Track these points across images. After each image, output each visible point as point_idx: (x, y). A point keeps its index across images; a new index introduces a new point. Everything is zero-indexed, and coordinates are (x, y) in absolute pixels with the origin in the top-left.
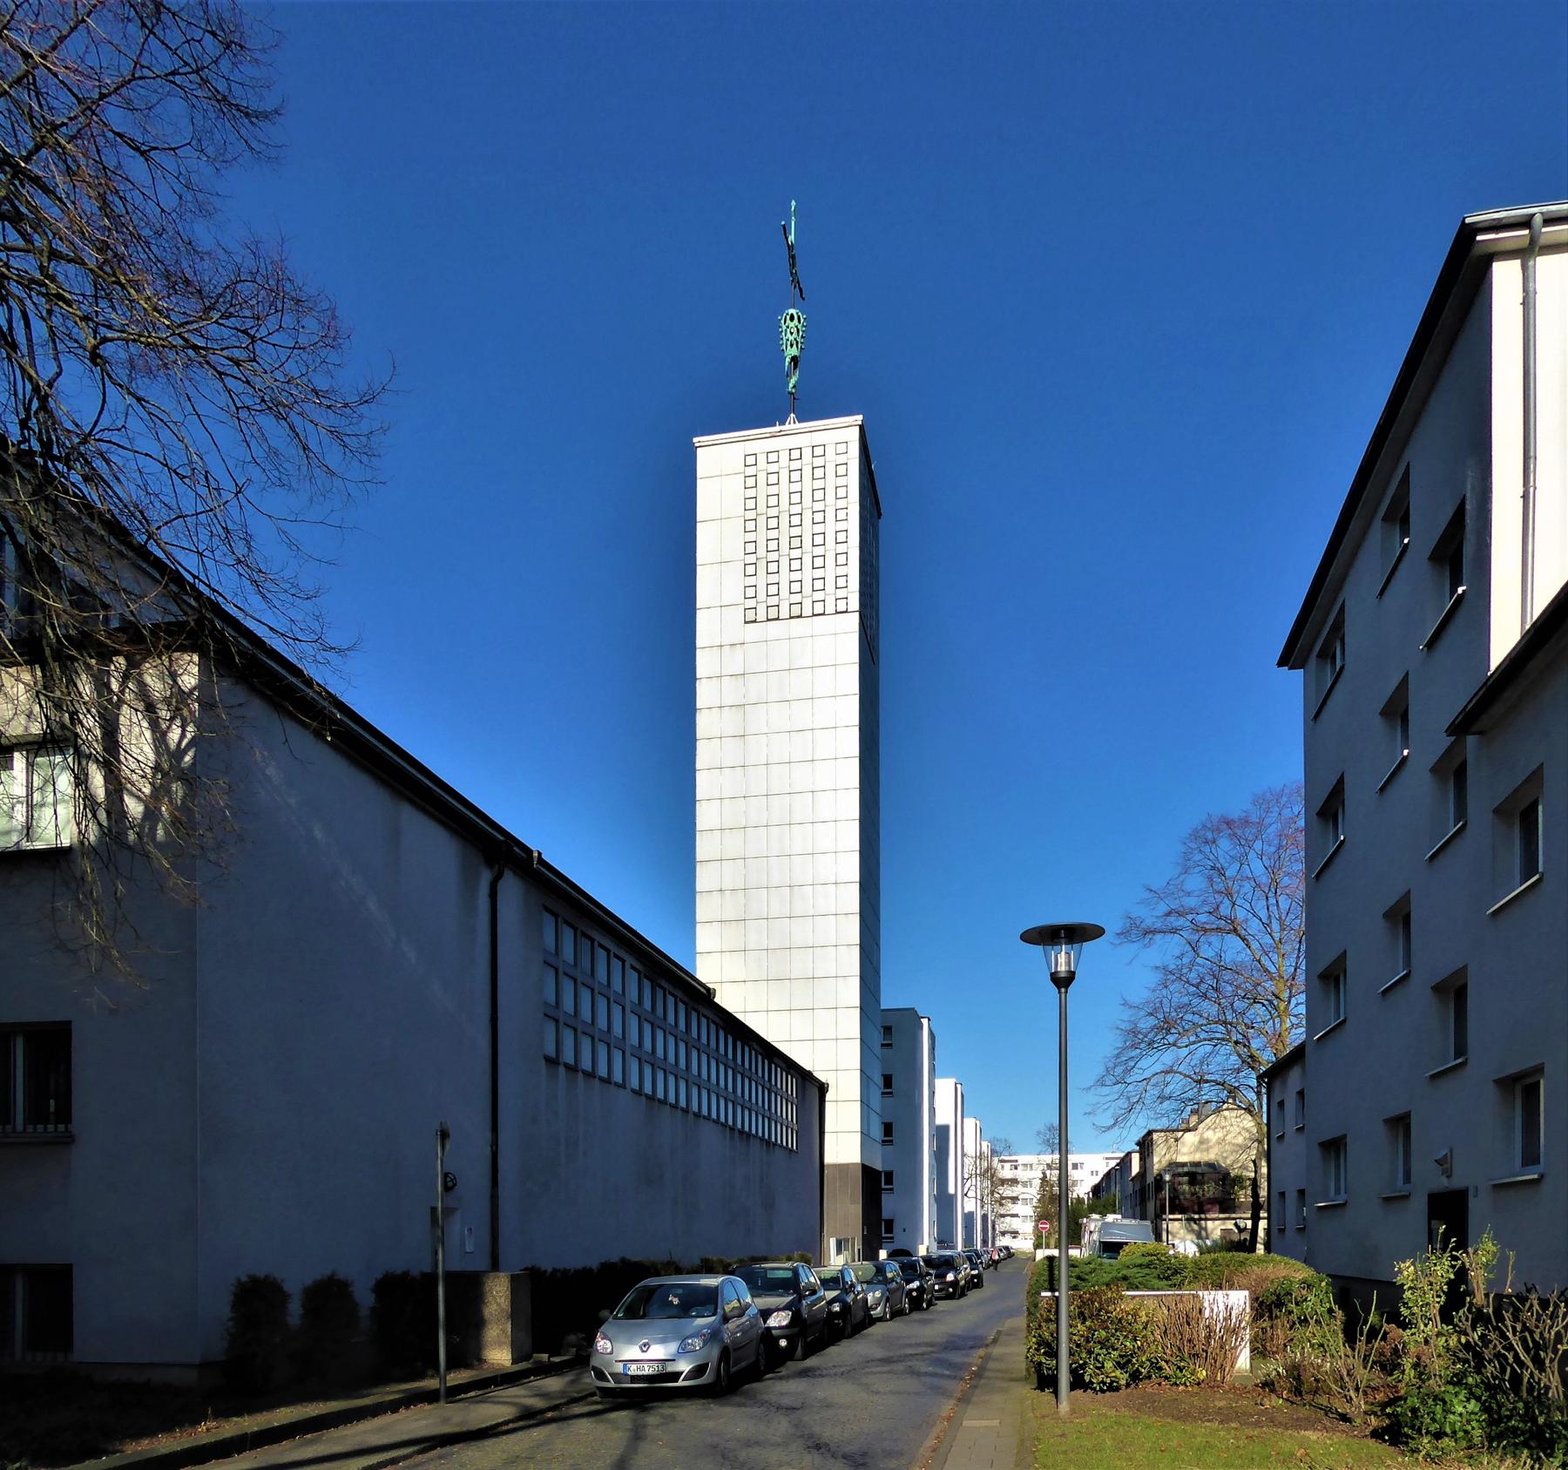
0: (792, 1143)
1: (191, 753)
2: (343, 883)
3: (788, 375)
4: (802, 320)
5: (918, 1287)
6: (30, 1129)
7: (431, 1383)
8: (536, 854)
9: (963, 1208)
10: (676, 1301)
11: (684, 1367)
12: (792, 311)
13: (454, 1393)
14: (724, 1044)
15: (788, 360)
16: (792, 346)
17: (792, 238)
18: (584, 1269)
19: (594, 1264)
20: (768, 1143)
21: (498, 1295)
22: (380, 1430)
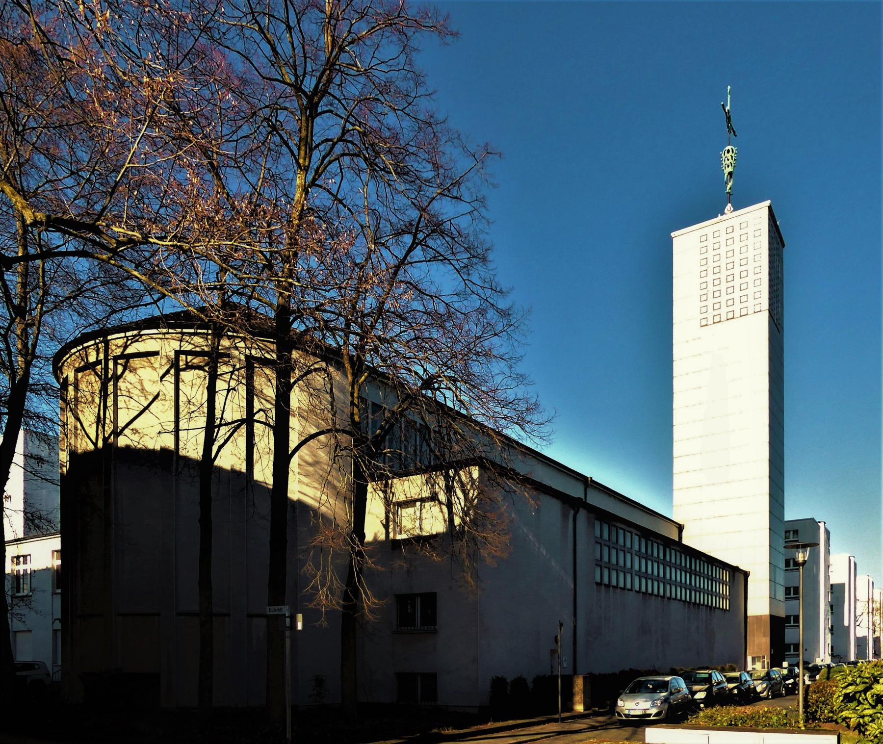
0: (725, 605)
1: (476, 501)
2: (521, 531)
3: (727, 183)
4: (734, 151)
5: (792, 683)
6: (422, 628)
7: (557, 716)
8: (590, 479)
9: (855, 634)
10: (651, 687)
11: (654, 711)
12: (729, 147)
13: (563, 720)
14: (685, 561)
15: (726, 175)
16: (728, 166)
17: (728, 108)
18: (365, 534)
19: (617, 671)
20: (711, 608)
21: (579, 684)
22: (542, 729)
